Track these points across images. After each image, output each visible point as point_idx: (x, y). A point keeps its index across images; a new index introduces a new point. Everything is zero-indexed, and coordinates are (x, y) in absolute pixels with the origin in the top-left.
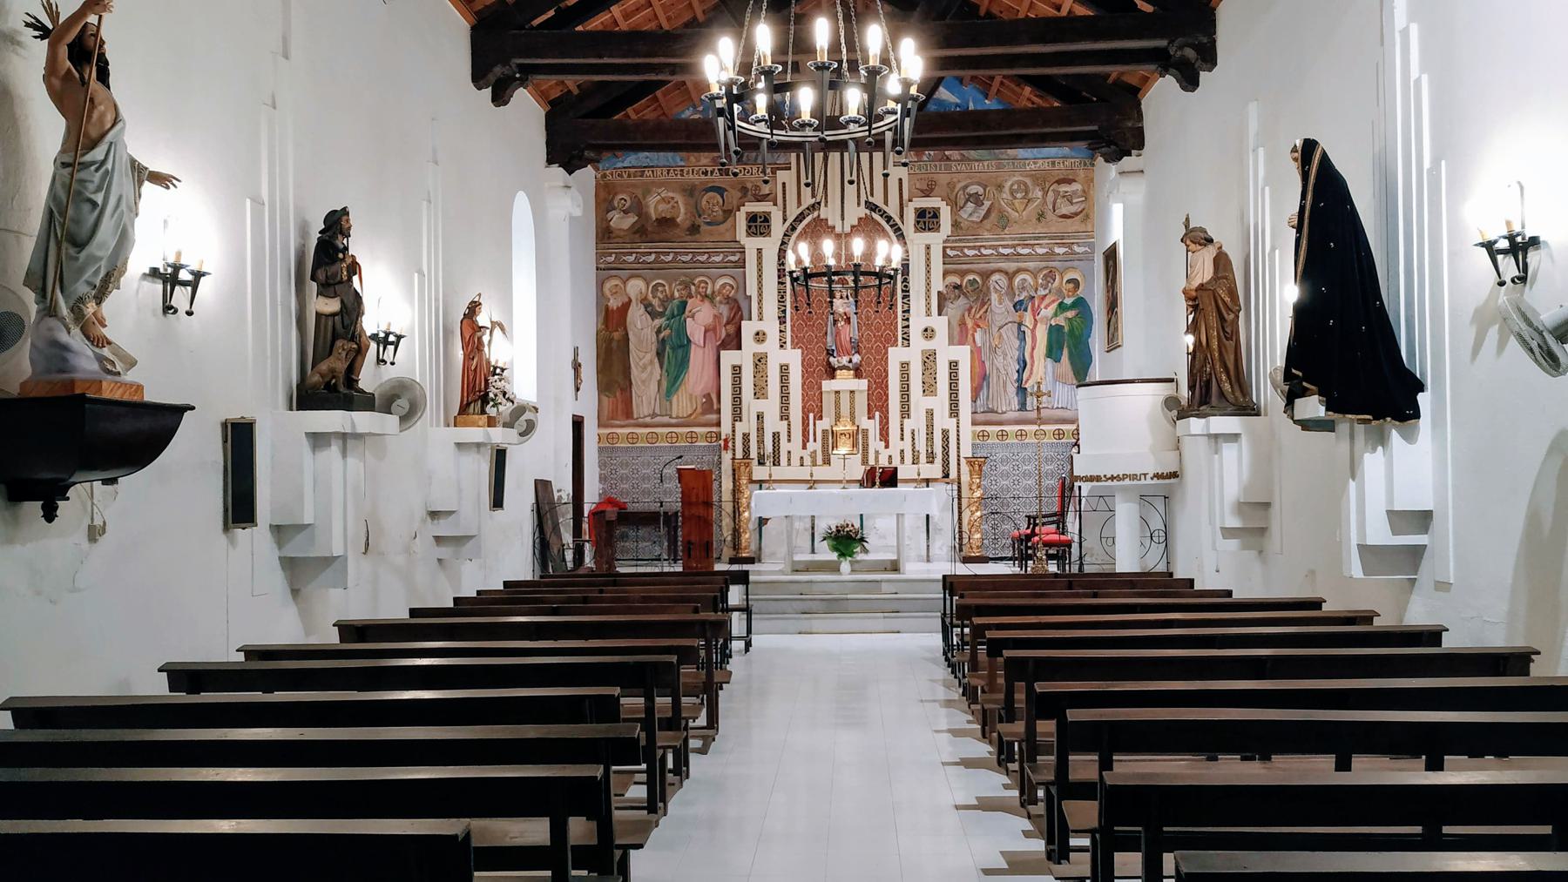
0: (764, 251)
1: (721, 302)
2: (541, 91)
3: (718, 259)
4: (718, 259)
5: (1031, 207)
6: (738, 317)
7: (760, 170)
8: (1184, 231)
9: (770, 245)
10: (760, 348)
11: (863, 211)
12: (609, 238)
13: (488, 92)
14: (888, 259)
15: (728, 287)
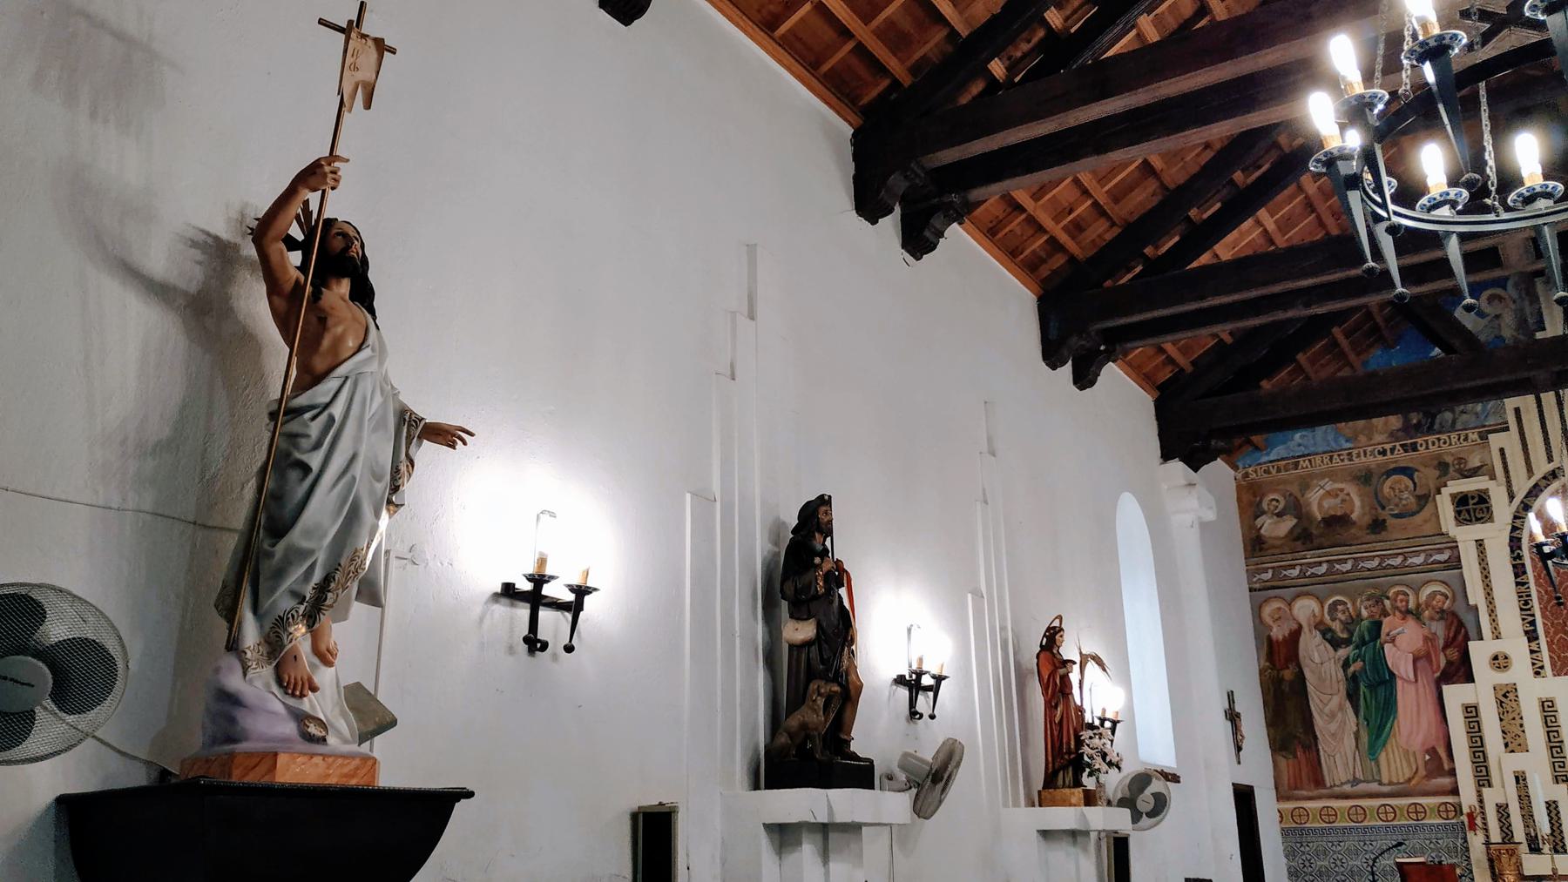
1: (1432, 619)
2: (1144, 374)
3: (1419, 560)
4: (1419, 560)
6: (1460, 637)
7: (1462, 438)
10: (1503, 678)
12: (1261, 550)
13: (1067, 370)
15: (1438, 597)
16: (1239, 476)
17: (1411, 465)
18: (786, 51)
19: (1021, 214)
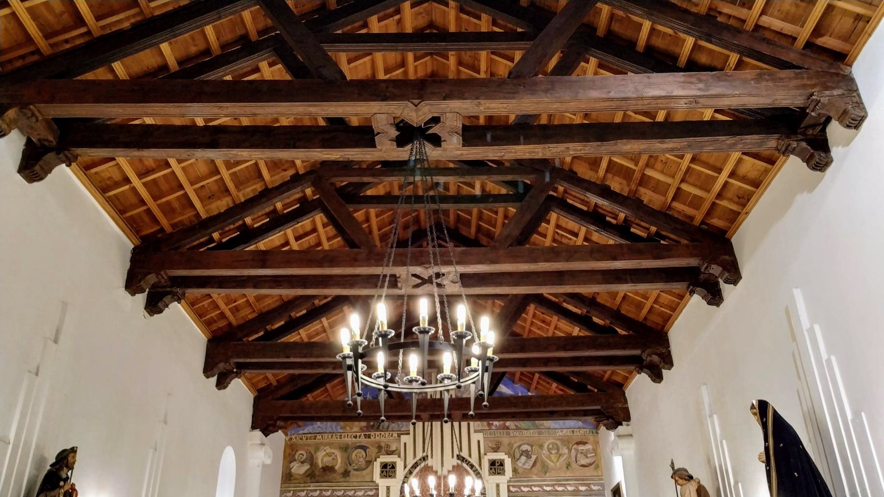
0: (391, 488)
5: (562, 459)
8: (672, 472)
9: (394, 484)
11: (455, 461)
12: (290, 480)
13: (214, 380)
14: (473, 491)
16: (287, 439)
17: (366, 445)
18: (110, 205)
19: (209, 299)
